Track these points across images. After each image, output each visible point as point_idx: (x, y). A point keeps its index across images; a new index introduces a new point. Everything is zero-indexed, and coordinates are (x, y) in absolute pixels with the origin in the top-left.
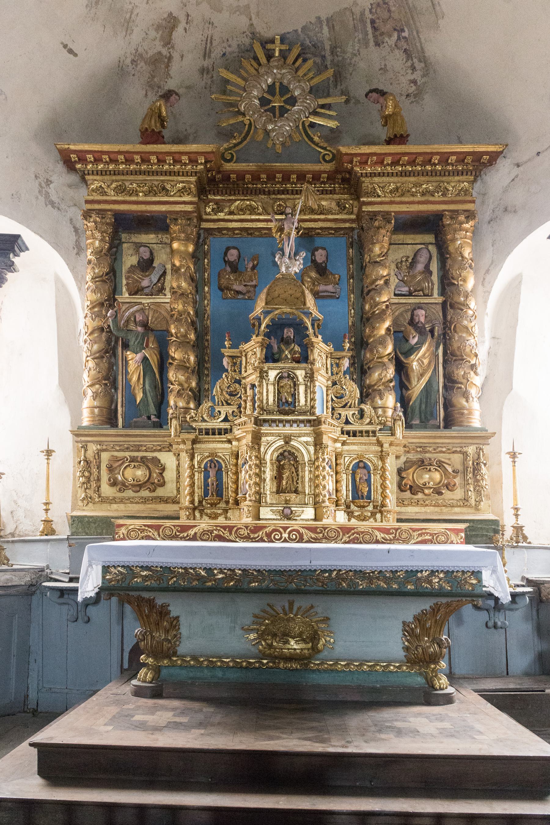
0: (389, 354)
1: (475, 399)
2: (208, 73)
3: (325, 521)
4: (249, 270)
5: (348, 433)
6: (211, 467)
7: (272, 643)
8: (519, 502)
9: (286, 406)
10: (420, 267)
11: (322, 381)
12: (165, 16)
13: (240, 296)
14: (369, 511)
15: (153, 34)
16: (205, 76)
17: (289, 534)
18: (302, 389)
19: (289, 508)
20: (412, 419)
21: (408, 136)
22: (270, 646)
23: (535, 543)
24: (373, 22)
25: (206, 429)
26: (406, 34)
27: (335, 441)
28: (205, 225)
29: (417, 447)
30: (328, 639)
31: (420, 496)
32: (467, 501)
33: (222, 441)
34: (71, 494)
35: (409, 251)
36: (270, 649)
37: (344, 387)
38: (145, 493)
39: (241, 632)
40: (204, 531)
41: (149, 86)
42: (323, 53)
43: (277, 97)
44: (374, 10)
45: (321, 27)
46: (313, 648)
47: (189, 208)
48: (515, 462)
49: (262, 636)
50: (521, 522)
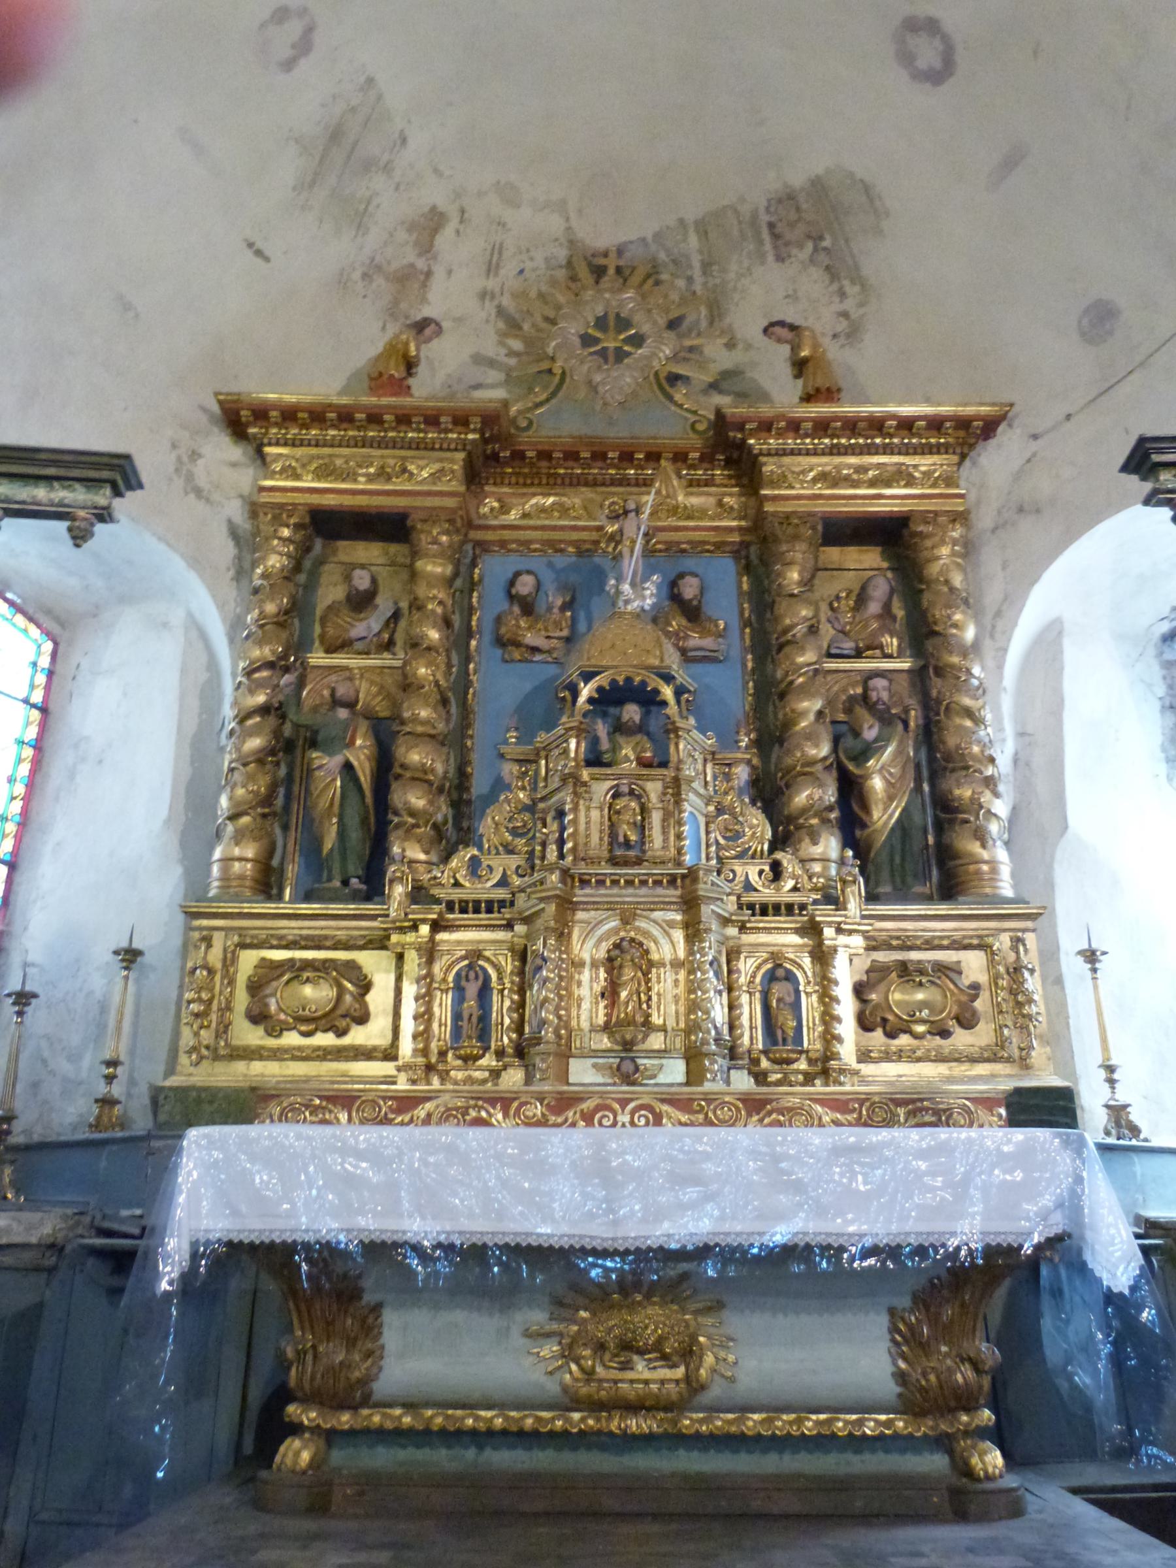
0: (825, 758)
1: (999, 843)
2: (493, 297)
3: (708, 1086)
4: (556, 610)
5: (751, 906)
6: (467, 980)
7: (593, 1367)
8: (1113, 1054)
9: (625, 852)
10: (874, 608)
11: (693, 805)
12: (426, 209)
13: (538, 657)
14: (798, 1072)
15: (402, 235)
16: (487, 303)
17: (632, 1113)
18: (656, 817)
19: (633, 1059)
20: (877, 884)
21: (839, 390)
22: (589, 1374)
23: (1155, 1143)
24: (771, 226)
25: (460, 901)
26: (826, 243)
27: (726, 921)
28: (475, 535)
29: (892, 937)
30: (722, 1354)
31: (904, 1040)
32: (1003, 1048)
33: (494, 926)
34: (166, 1048)
35: (849, 580)
36: (588, 1381)
37: (740, 819)
38: (325, 1039)
39: (524, 1341)
40: (448, 1109)
41: (392, 315)
42: (689, 273)
43: (611, 334)
44: (772, 209)
45: (685, 235)
46: (687, 1379)
47: (451, 503)
48: (1094, 970)
49: (569, 1354)
50: (1122, 1097)
